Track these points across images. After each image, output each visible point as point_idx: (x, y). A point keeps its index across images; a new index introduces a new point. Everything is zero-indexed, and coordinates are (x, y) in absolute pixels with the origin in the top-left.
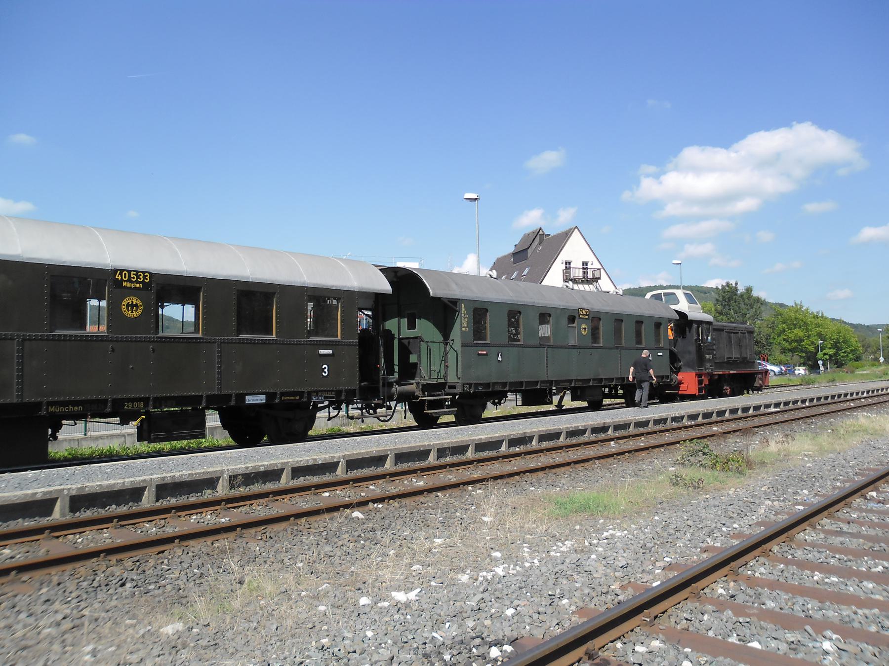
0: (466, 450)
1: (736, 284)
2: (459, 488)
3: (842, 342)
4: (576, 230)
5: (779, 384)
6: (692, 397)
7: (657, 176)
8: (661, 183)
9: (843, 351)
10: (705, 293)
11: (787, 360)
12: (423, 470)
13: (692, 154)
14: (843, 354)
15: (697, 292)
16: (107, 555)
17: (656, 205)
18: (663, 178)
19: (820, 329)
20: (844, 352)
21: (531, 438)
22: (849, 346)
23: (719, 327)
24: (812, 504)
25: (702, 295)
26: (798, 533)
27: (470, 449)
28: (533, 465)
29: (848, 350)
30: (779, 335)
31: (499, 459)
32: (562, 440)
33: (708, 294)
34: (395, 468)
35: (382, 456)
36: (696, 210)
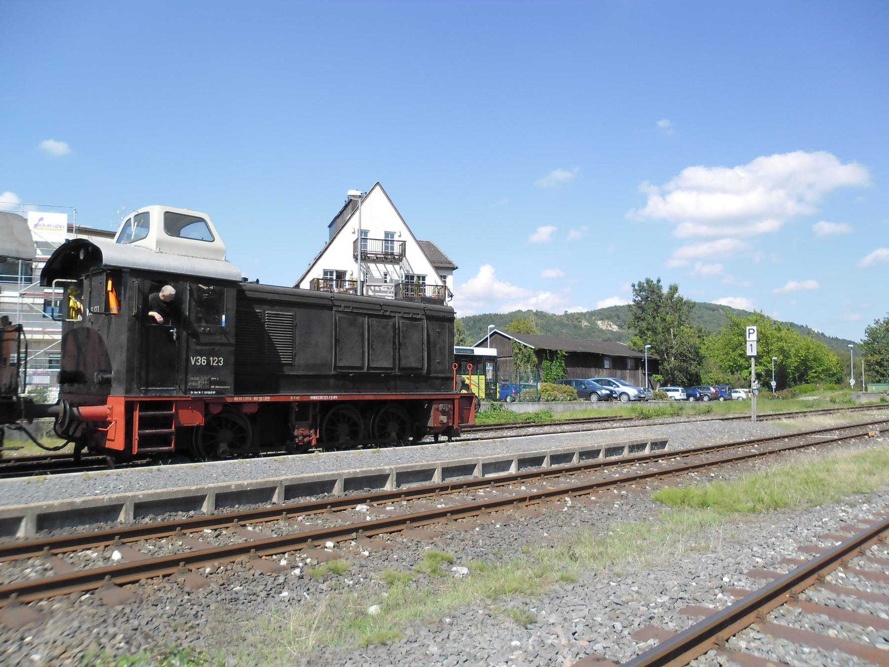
0: (330, 490)
1: (659, 281)
2: (513, 505)
3: (812, 360)
4: (378, 187)
5: (596, 416)
6: (123, 459)
7: (663, 194)
8: (665, 202)
9: (814, 371)
10: (714, 311)
11: (729, 380)
12: (567, 470)
13: (696, 174)
14: (813, 374)
15: (705, 310)
16: (111, 577)
17: (668, 225)
18: (668, 198)
19: (781, 344)
20: (815, 372)
21: (597, 452)
22: (821, 365)
23: (277, 297)
24: (752, 593)
25: (710, 312)
26: (706, 653)
27: (336, 486)
28: (551, 488)
29: (820, 369)
30: (734, 351)
31: (463, 488)
32: (545, 465)
33: (716, 312)
34: (216, 512)
35: (114, 506)
36: (704, 230)
